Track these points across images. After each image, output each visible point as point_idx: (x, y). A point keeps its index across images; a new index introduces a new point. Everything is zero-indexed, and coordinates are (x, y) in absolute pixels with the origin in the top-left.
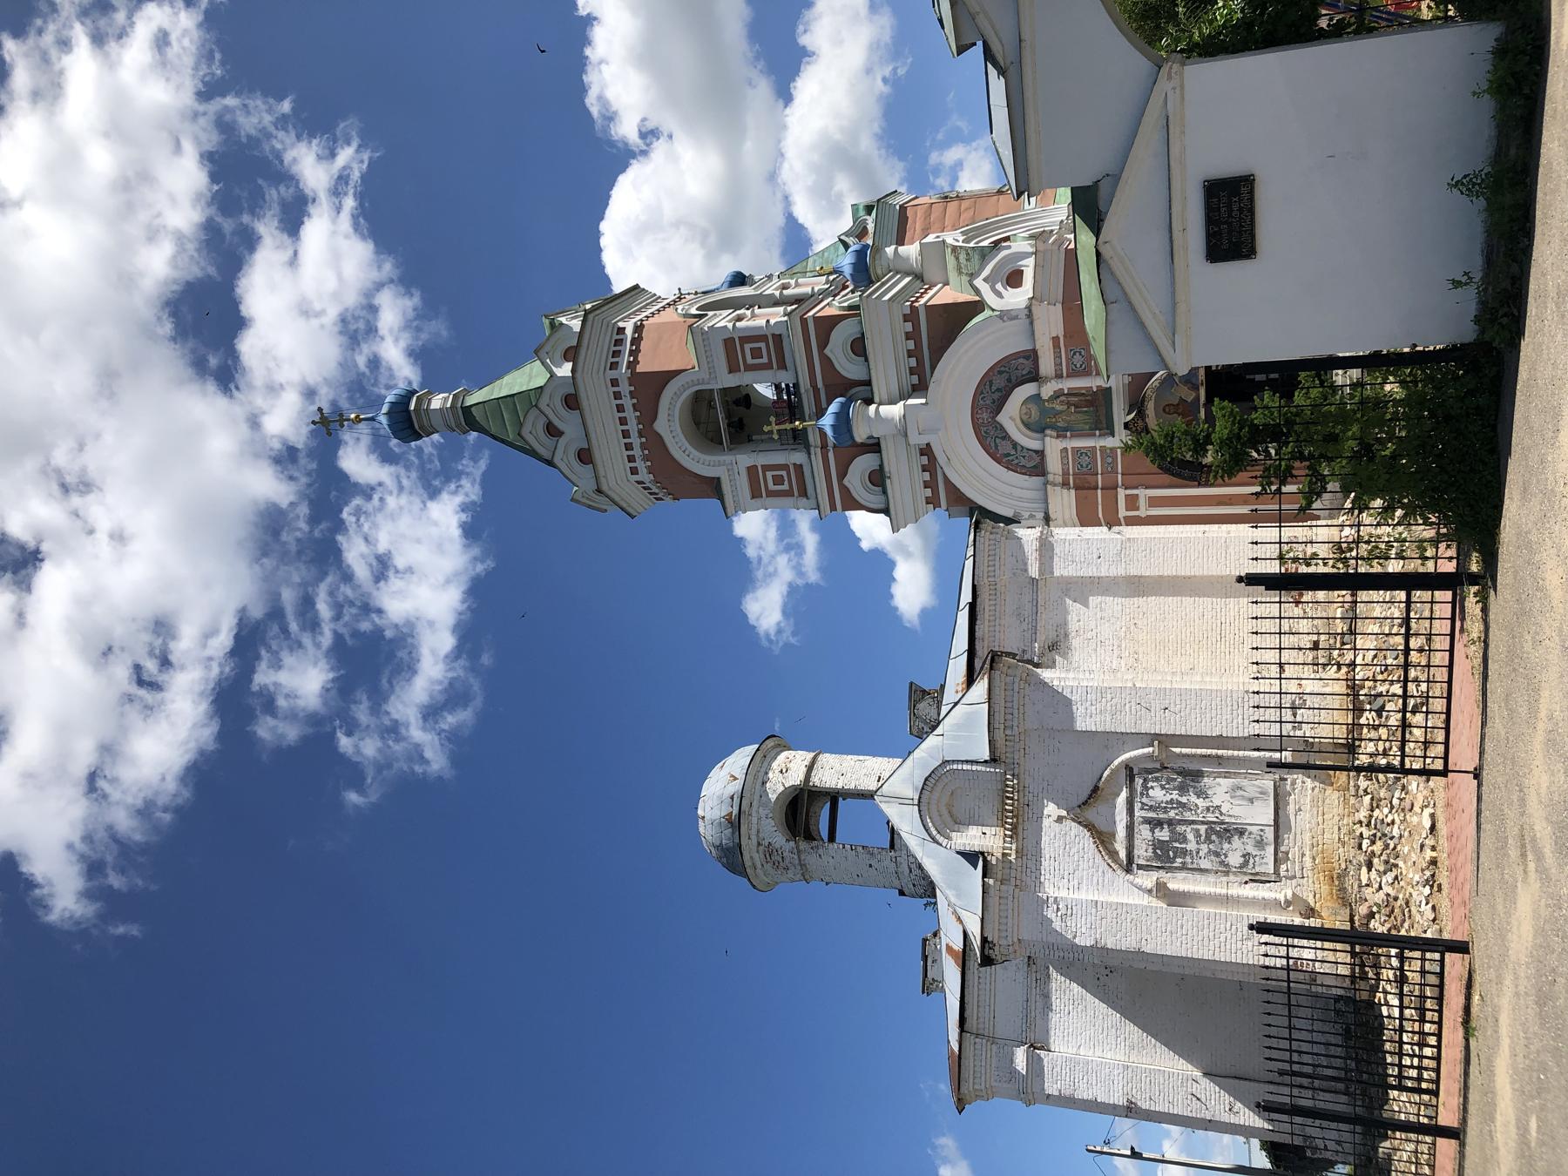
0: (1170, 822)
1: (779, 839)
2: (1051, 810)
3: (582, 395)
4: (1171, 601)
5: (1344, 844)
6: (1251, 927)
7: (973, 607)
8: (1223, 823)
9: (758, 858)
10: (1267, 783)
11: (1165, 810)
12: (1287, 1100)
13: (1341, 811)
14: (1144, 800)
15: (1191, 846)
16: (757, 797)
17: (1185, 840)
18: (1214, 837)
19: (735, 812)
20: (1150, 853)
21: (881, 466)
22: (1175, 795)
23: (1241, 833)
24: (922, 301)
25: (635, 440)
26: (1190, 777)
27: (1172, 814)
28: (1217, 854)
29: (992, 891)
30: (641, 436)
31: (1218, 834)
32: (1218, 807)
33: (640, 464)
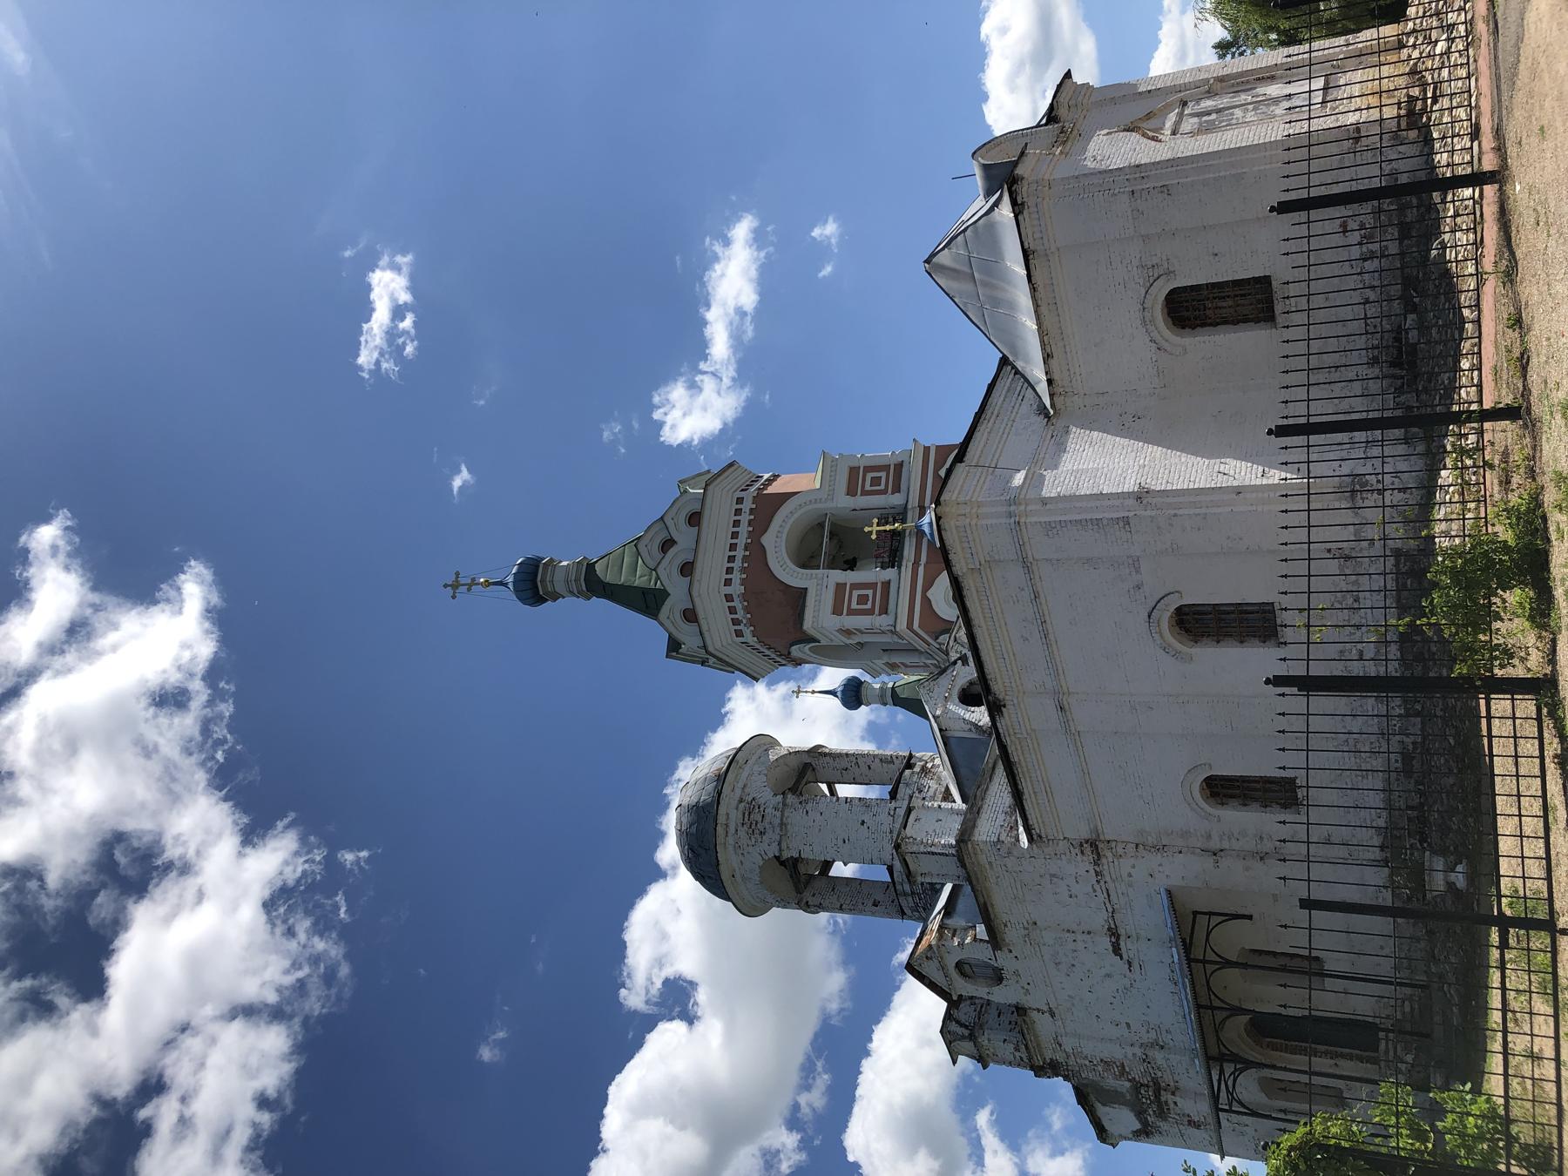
3: (698, 566)
9: (735, 816)
30: (746, 549)
33: (736, 577)
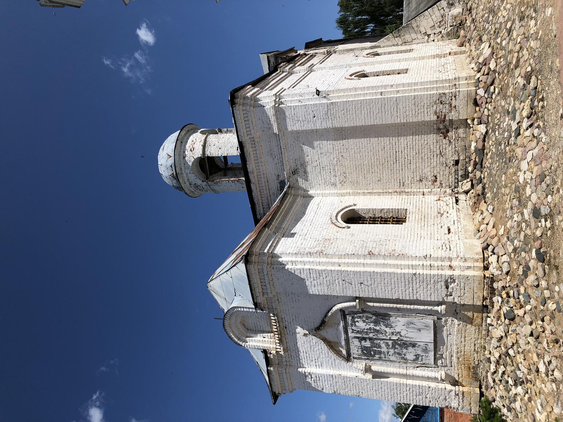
0: (370, 339)
2: (299, 329)
4: (364, 141)
5: (477, 352)
8: (402, 340)
10: (429, 321)
11: (367, 333)
13: (476, 336)
14: (354, 328)
16: (183, 165)
17: (380, 347)
18: (397, 346)
19: (175, 173)
22: (372, 325)
23: (414, 345)
26: (382, 317)
27: (371, 335)
28: (400, 354)
29: (274, 373)
31: (399, 345)
32: (399, 333)
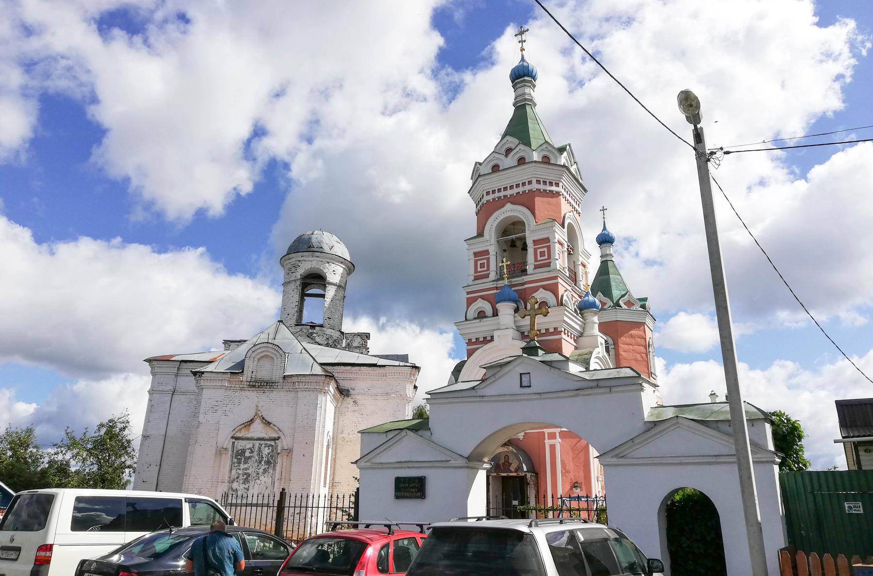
1: (301, 271)
6: (283, 489)
7: (375, 365)
12: (287, 504)
15: (242, 466)
20: (240, 448)
21: (487, 317)
24: (564, 336)
25: (502, 194)
28: (238, 478)
